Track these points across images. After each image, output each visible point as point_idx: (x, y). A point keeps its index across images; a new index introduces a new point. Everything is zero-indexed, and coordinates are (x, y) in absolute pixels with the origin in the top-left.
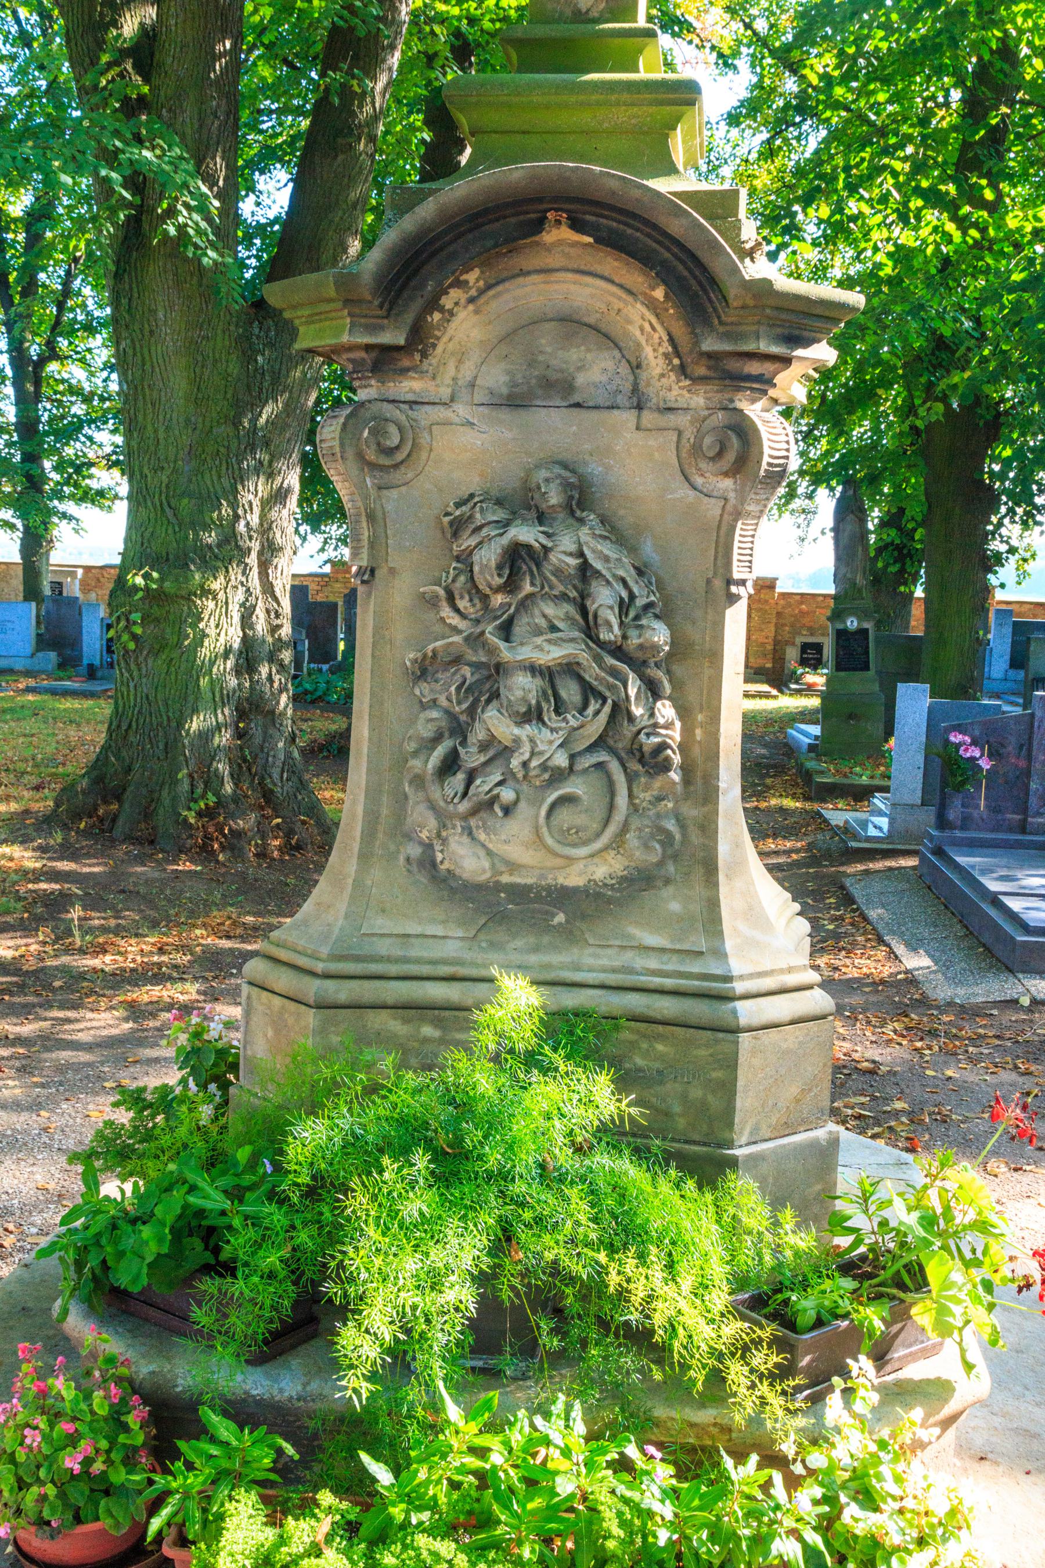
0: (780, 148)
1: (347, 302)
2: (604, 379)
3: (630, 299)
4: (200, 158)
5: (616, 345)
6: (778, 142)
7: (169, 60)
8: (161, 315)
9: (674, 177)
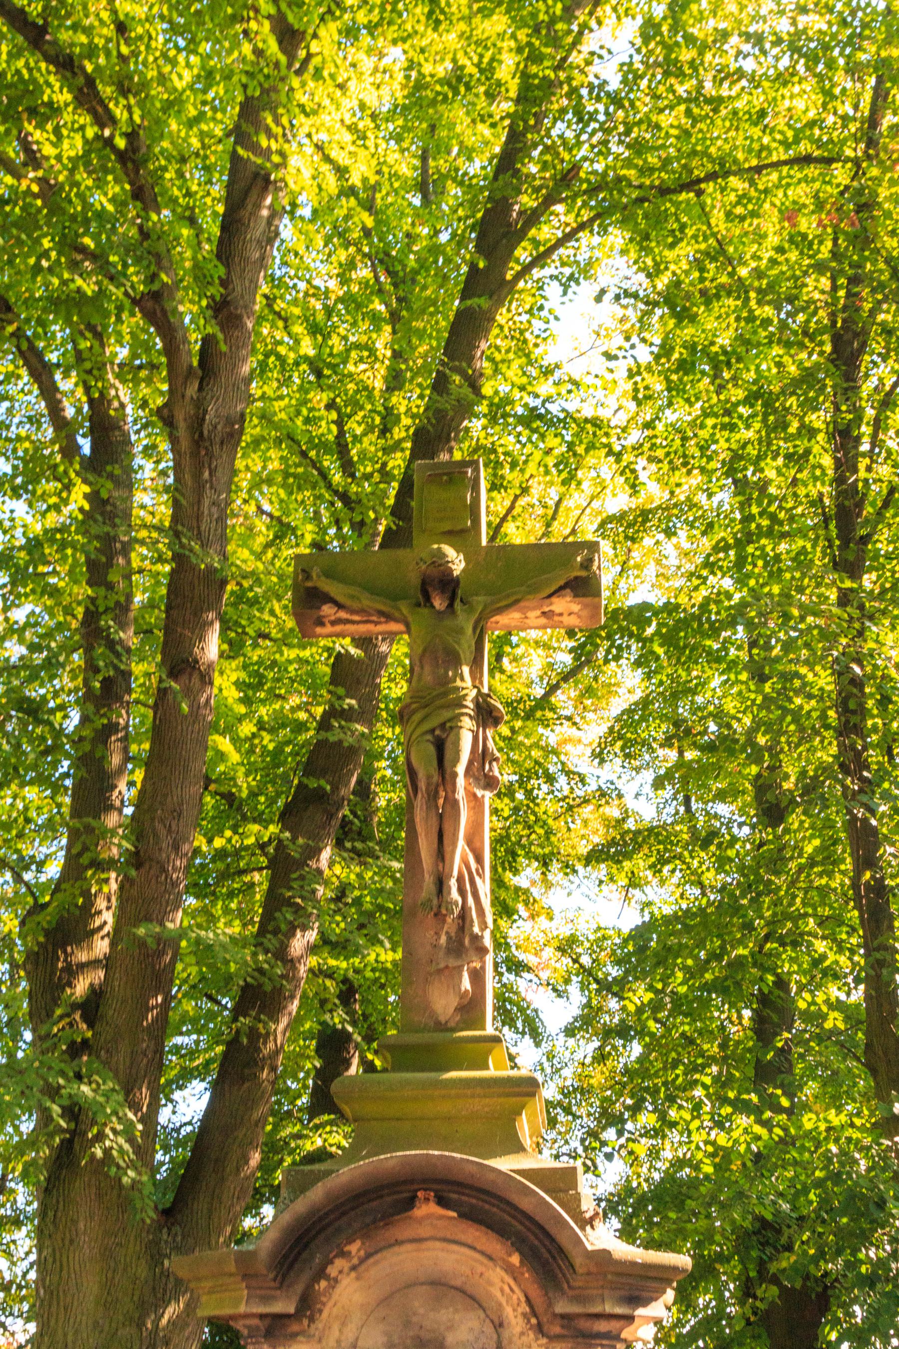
0: (609, 1054)
1: (245, 1277)
2: (471, 1338)
3: (491, 1264)
4: (129, 1089)
5: (480, 1306)
6: (608, 1048)
7: (111, 1012)
8: (81, 1225)
9: (522, 1154)
